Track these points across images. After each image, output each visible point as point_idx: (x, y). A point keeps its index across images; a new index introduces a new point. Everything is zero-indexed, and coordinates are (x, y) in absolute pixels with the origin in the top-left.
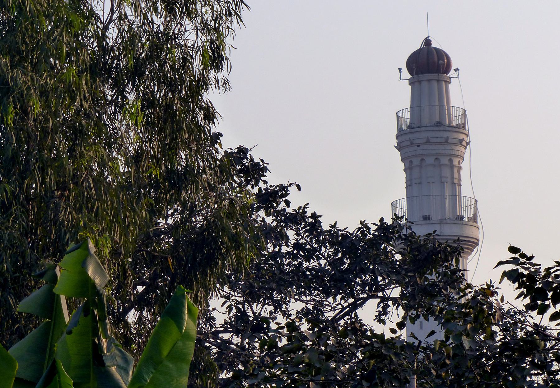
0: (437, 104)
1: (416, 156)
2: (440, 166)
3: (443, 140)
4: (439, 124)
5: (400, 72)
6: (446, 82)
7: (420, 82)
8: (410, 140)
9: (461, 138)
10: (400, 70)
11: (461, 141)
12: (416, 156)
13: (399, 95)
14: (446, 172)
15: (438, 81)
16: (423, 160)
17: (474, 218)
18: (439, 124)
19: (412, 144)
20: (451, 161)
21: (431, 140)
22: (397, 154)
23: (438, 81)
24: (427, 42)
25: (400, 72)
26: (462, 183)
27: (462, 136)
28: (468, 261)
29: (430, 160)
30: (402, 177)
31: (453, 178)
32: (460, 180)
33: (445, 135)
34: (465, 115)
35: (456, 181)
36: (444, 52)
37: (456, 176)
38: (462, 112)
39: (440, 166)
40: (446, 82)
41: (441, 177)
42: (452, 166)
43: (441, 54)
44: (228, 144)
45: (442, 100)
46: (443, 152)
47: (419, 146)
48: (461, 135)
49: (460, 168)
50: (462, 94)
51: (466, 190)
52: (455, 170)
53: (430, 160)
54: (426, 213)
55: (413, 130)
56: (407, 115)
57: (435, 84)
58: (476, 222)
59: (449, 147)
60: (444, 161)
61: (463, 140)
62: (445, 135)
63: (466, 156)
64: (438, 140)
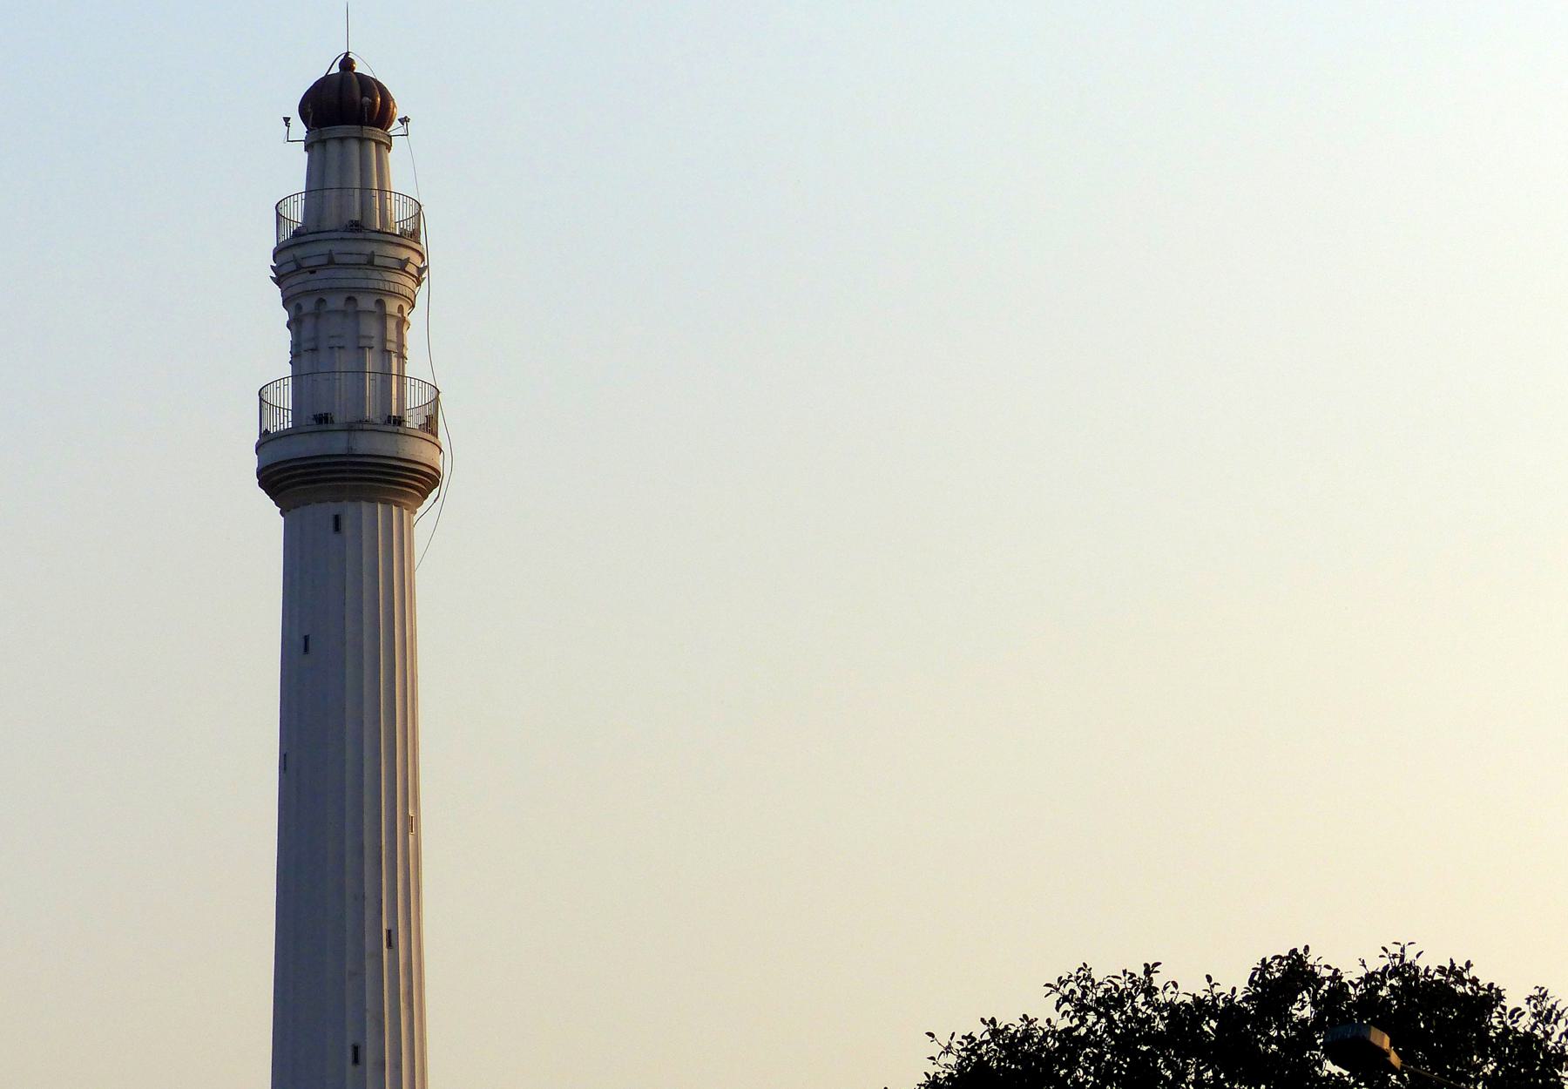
0: (357, 184)
1: (307, 293)
2: (357, 313)
3: (363, 260)
4: (357, 227)
5: (287, 124)
6: (378, 143)
7: (323, 142)
8: (295, 260)
9: (404, 257)
10: (287, 120)
11: (403, 265)
12: (307, 293)
13: (284, 168)
14: (370, 327)
15: (362, 140)
16: (321, 301)
17: (430, 425)
18: (357, 227)
19: (299, 268)
20: (381, 303)
21: (338, 259)
22: (276, 292)
23: (362, 140)
24: (347, 63)
25: (287, 124)
26: (407, 354)
27: (405, 254)
28: (416, 518)
29: (336, 302)
30: (283, 339)
31: (384, 340)
32: (401, 345)
33: (369, 248)
34: (418, 214)
35: (391, 346)
36: (379, 84)
37: (392, 334)
38: (411, 212)
39: (357, 313)
40: (378, 143)
41: (359, 337)
42: (383, 316)
43: (369, 85)
44: (1242, 985)
45: (371, 185)
46: (363, 284)
47: (313, 272)
48: (402, 249)
49: (402, 322)
50: (414, 170)
51: (415, 366)
52: (392, 325)
53: (336, 302)
54: (323, 410)
55: (303, 239)
56: (296, 213)
57: (354, 147)
58: (436, 435)
59: (375, 275)
60: (366, 303)
61: (407, 261)
62: (369, 248)
63: (421, 301)
64: (347, 259)
